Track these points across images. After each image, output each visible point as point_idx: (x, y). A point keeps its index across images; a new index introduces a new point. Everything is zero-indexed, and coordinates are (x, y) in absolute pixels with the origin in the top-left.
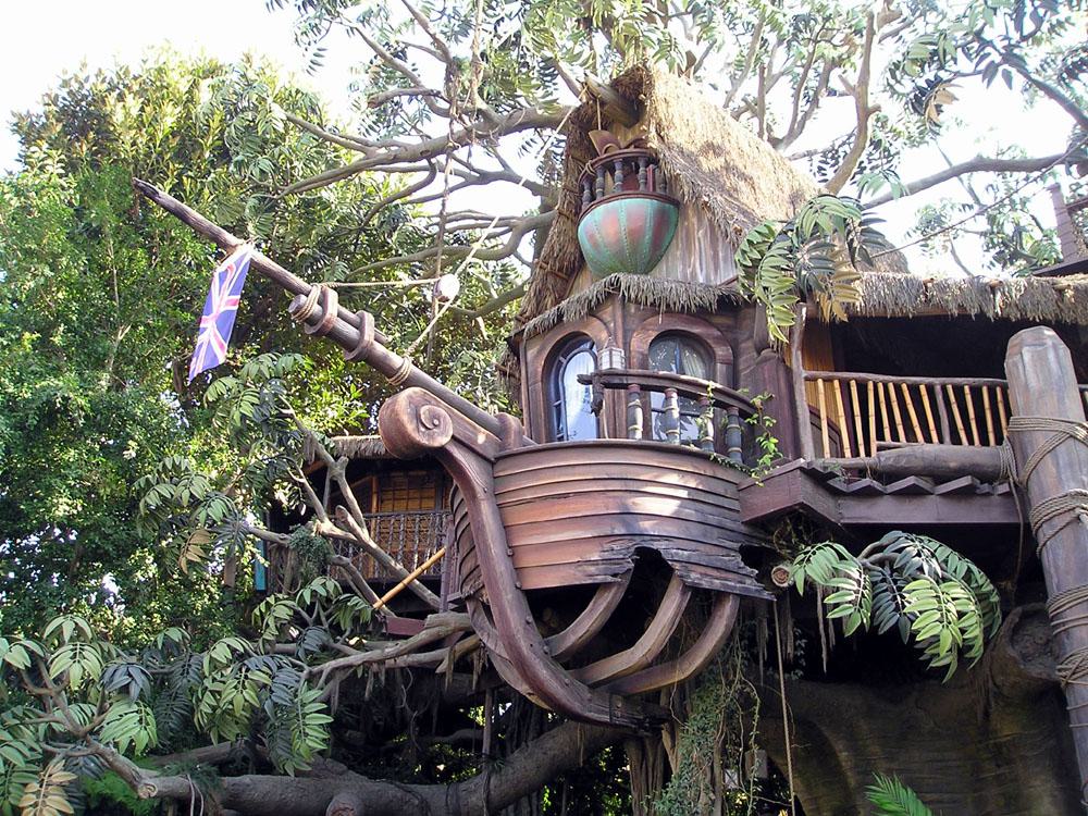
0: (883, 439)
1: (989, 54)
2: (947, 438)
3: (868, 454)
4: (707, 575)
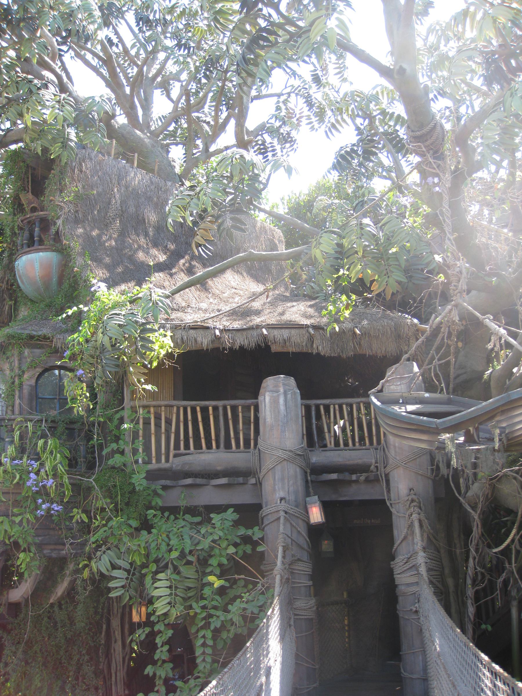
0: (179, 449)
1: (472, 31)
2: (222, 445)
3: (167, 460)
4: (55, 549)
